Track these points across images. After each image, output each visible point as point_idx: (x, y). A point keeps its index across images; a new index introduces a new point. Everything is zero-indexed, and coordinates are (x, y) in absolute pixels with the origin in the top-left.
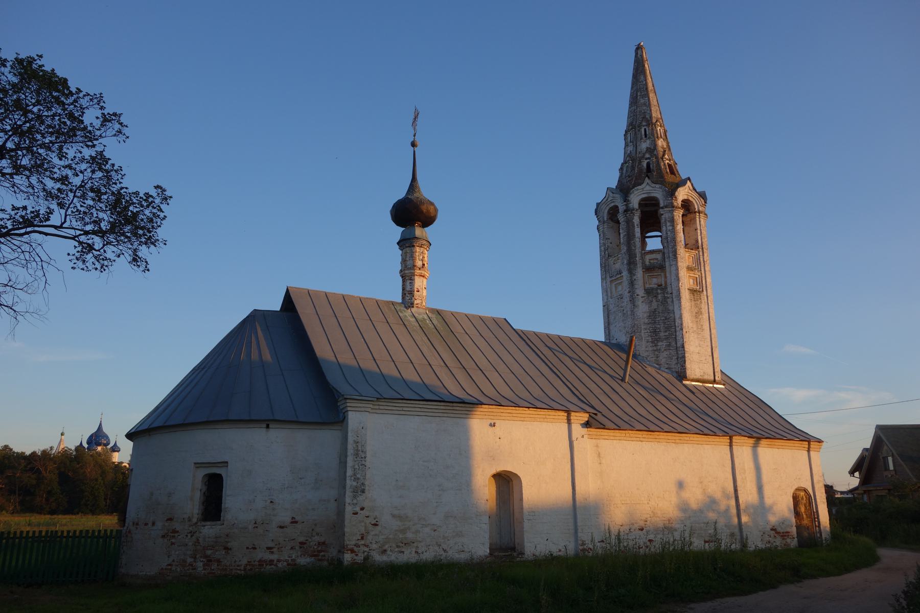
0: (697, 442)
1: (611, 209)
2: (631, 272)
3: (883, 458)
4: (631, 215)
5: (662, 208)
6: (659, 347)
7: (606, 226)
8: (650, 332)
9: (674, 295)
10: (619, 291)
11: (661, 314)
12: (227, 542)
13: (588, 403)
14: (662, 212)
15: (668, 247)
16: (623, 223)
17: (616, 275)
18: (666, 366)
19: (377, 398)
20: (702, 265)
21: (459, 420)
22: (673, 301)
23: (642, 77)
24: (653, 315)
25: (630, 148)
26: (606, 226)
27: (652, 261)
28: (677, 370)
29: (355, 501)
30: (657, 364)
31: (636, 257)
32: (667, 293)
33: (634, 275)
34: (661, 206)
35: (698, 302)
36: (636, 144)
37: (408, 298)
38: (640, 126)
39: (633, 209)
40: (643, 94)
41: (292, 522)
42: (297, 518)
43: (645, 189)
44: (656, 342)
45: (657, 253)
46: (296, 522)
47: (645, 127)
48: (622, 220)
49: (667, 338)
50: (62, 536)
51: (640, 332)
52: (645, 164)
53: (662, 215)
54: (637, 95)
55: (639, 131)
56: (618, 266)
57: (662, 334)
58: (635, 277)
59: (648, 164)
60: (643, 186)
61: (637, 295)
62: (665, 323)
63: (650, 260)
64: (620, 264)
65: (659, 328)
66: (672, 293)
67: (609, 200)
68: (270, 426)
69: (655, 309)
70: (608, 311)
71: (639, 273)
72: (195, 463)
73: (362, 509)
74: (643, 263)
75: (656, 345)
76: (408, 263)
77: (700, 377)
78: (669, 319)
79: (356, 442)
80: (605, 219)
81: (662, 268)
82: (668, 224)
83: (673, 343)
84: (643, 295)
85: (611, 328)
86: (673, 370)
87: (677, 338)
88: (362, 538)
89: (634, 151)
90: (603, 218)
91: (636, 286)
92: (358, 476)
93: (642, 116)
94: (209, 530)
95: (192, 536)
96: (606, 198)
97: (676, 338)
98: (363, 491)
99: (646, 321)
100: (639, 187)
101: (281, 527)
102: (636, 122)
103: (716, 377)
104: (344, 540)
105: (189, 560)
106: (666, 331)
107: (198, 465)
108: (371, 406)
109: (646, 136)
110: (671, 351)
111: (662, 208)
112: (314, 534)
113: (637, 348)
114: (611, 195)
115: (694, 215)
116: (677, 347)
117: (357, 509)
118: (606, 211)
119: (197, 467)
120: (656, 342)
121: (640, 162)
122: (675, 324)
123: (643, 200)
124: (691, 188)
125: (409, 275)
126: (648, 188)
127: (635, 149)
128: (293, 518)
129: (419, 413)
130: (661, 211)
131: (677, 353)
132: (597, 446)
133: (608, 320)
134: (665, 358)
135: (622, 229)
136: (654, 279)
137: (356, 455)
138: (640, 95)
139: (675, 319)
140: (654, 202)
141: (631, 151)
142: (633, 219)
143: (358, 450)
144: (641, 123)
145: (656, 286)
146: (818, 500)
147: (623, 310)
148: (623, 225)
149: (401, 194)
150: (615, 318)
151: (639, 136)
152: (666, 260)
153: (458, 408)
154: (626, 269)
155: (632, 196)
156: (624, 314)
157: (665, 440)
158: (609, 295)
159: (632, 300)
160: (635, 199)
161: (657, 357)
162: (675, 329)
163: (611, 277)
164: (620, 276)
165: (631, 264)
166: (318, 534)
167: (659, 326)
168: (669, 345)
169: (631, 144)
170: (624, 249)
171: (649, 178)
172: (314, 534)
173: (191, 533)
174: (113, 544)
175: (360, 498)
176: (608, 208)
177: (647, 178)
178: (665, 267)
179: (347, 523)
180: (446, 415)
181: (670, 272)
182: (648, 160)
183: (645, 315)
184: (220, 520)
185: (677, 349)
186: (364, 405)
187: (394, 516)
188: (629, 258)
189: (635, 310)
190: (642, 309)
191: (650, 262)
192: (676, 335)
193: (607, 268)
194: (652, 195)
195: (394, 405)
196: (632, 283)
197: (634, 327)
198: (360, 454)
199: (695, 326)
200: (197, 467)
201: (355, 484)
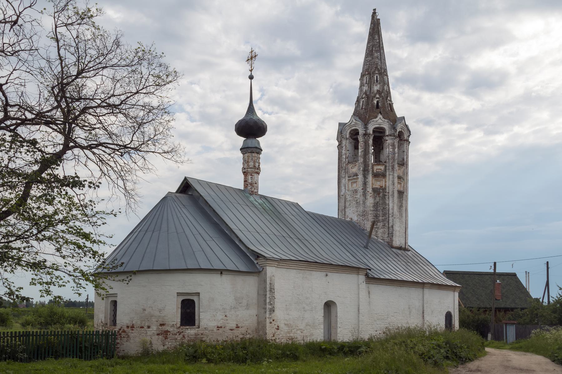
2: (365, 177)
4: (368, 138)
5: (387, 136)
6: (378, 226)
7: (348, 142)
8: (374, 216)
9: (390, 194)
10: (354, 187)
11: (381, 205)
12: (203, 338)
13: (363, 262)
14: (387, 139)
15: (389, 162)
16: (362, 142)
17: (354, 176)
18: (381, 238)
20: (405, 175)
22: (389, 198)
23: (376, 37)
24: (376, 205)
25: (365, 88)
26: (348, 142)
27: (377, 170)
29: (270, 317)
30: (376, 237)
31: (369, 167)
32: (386, 192)
33: (367, 178)
34: (387, 134)
35: (401, 199)
36: (371, 86)
37: (249, 188)
38: (374, 73)
39: (370, 134)
40: (376, 49)
41: (236, 327)
42: (239, 325)
43: (378, 122)
46: (238, 327)
47: (377, 75)
48: (361, 140)
49: (383, 221)
50: (93, 334)
51: (368, 216)
52: (375, 102)
53: (387, 140)
54: (373, 49)
55: (373, 76)
56: (355, 170)
57: (381, 218)
58: (367, 180)
59: (378, 102)
61: (368, 192)
62: (383, 211)
63: (376, 169)
64: (355, 169)
65: (379, 214)
66: (388, 193)
67: (352, 124)
68: (223, 273)
69: (378, 202)
70: (345, 199)
71: (370, 178)
72: (177, 293)
73: (273, 320)
74: (373, 171)
76: (250, 164)
78: (385, 209)
80: (348, 137)
81: (384, 175)
82: (390, 147)
83: (387, 225)
84: (371, 192)
85: (346, 211)
86: (385, 241)
87: (390, 221)
88: (274, 336)
89: (369, 91)
90: (346, 136)
91: (368, 186)
92: (272, 302)
93: (375, 66)
94: (191, 332)
95: (179, 334)
97: (388, 221)
98: (274, 311)
99: (372, 209)
100: (375, 120)
101: (231, 330)
102: (371, 70)
104: (266, 337)
106: (383, 217)
107: (179, 294)
108: (277, 263)
109: (377, 82)
110: (385, 229)
111: (387, 136)
112: (247, 333)
113: (365, 226)
115: (404, 142)
116: (389, 227)
117: (272, 320)
118: (349, 131)
121: (372, 100)
123: (375, 128)
124: (404, 124)
125: (251, 172)
126: (380, 121)
127: (369, 89)
128: (237, 325)
129: (296, 268)
131: (389, 231)
132: (368, 287)
133: (345, 205)
134: (381, 233)
135: (361, 147)
136: (378, 182)
137: (271, 291)
138: (374, 50)
139: (389, 209)
141: (366, 90)
142: (369, 141)
143: (271, 288)
144: (374, 71)
145: (379, 187)
146: (455, 318)
147: (357, 200)
150: (350, 205)
151: (373, 80)
152: (387, 171)
154: (361, 174)
155: (370, 125)
156: (357, 202)
158: (347, 188)
159: (364, 194)
161: (376, 232)
162: (389, 215)
163: (349, 177)
164: (356, 177)
165: (365, 171)
166: (249, 334)
167: (379, 213)
168: (384, 225)
169: (367, 85)
170: (361, 160)
171: (381, 114)
172: (247, 333)
173: (179, 332)
174: (63, 339)
175: (273, 315)
176: (350, 130)
177: (380, 114)
178: (386, 175)
180: (307, 269)
181: (389, 180)
182: (378, 100)
183: (372, 205)
184: (195, 325)
185: (388, 228)
187: (285, 325)
188: (365, 167)
189: (365, 202)
190: (370, 201)
191: (376, 171)
192: (389, 219)
193: (346, 171)
194: (382, 126)
195: (286, 263)
196: (365, 183)
197: (364, 212)
198: (272, 290)
199: (399, 215)
201: (270, 307)
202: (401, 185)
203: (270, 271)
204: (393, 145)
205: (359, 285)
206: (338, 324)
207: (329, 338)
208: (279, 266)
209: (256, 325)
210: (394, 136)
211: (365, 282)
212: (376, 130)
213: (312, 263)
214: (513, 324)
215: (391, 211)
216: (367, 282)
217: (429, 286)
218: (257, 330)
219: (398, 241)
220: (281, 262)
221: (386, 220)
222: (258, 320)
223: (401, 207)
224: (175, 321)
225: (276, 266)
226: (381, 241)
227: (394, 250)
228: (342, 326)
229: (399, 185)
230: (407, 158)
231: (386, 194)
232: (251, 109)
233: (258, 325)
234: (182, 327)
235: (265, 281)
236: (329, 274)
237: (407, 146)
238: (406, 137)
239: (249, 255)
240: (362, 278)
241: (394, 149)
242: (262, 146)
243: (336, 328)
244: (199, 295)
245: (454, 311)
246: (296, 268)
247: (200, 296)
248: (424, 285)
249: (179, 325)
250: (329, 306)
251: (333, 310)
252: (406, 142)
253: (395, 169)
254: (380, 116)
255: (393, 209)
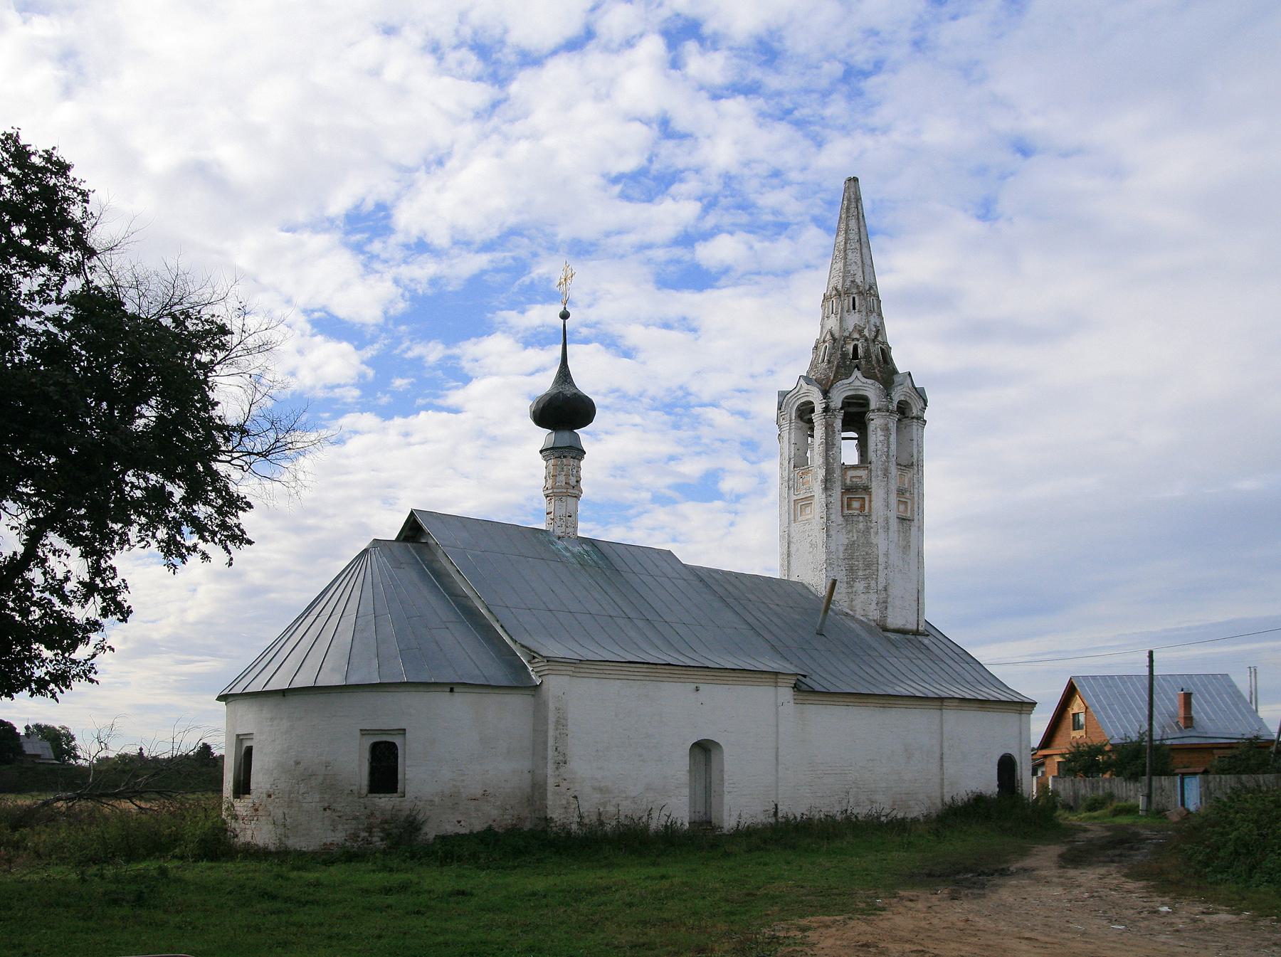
0: (905, 706)
1: (804, 404)
3: (1074, 715)
5: (873, 411)
19: (580, 660)
21: (659, 683)
27: (854, 480)
28: (875, 618)
44: (852, 583)
45: (862, 469)
47: (854, 295)
52: (850, 348)
57: (860, 573)
59: (855, 348)
60: (851, 380)
63: (851, 477)
68: (455, 690)
72: (361, 730)
74: (844, 480)
75: (852, 587)
77: (902, 627)
79: (558, 709)
81: (866, 489)
84: (840, 523)
94: (384, 802)
96: (797, 390)
97: (877, 579)
103: (920, 626)
105: (364, 834)
107: (364, 732)
108: (573, 669)
109: (854, 308)
114: (805, 385)
119: (363, 734)
120: (852, 583)
122: (877, 561)
130: (871, 415)
140: (861, 401)
148: (819, 431)
149: (545, 383)
152: (873, 479)
153: (661, 671)
157: (873, 705)
160: (837, 399)
167: (856, 563)
168: (868, 587)
171: (859, 370)
179: (549, 795)
180: (648, 678)
184: (396, 792)
186: (565, 668)
191: (851, 481)
195: (593, 667)
198: (561, 723)
200: (363, 734)
202: (906, 508)
203: (555, 685)
204: (886, 429)
205: (777, 707)
206: (726, 784)
207: (708, 813)
208: (575, 674)
209: (529, 790)
210: (888, 411)
211: (792, 701)
212: (847, 403)
213: (658, 667)
214: (1195, 774)
215: (882, 560)
216: (797, 701)
217: (957, 704)
218: (530, 801)
219: (899, 618)
220: (579, 665)
221: (871, 575)
222: (532, 780)
223: (906, 548)
224: (355, 785)
225: (571, 673)
226: (861, 618)
227: (889, 634)
228: (735, 789)
229: (902, 507)
230: (920, 452)
231: (873, 525)
232: (564, 375)
233: (532, 791)
234: (370, 795)
235: (545, 704)
236: (701, 687)
237: (920, 429)
238: (915, 412)
239: (519, 655)
240: (786, 693)
241: (887, 437)
242: (585, 445)
243: (721, 796)
244: (405, 734)
245: (1021, 756)
246: (623, 677)
247: (407, 735)
248: (942, 702)
249: (365, 790)
250: (704, 750)
251: (714, 756)
252: (915, 420)
253: (890, 475)
254: (857, 373)
255: (886, 555)
